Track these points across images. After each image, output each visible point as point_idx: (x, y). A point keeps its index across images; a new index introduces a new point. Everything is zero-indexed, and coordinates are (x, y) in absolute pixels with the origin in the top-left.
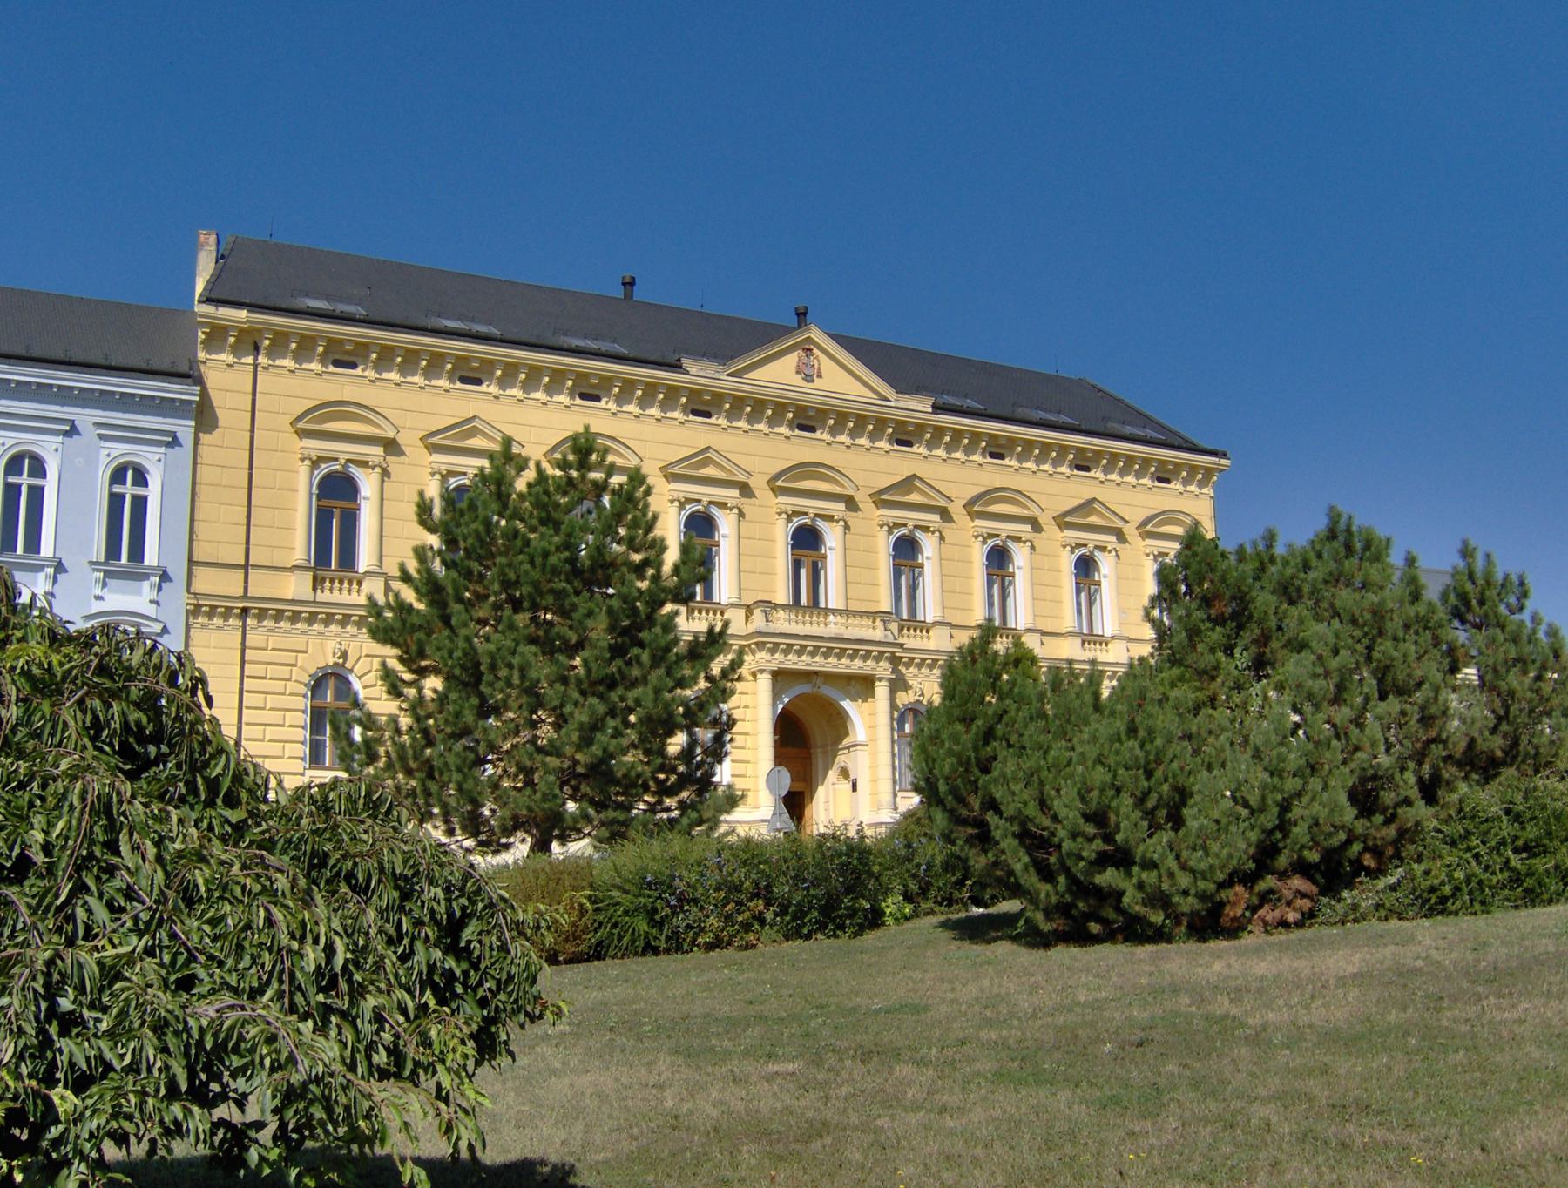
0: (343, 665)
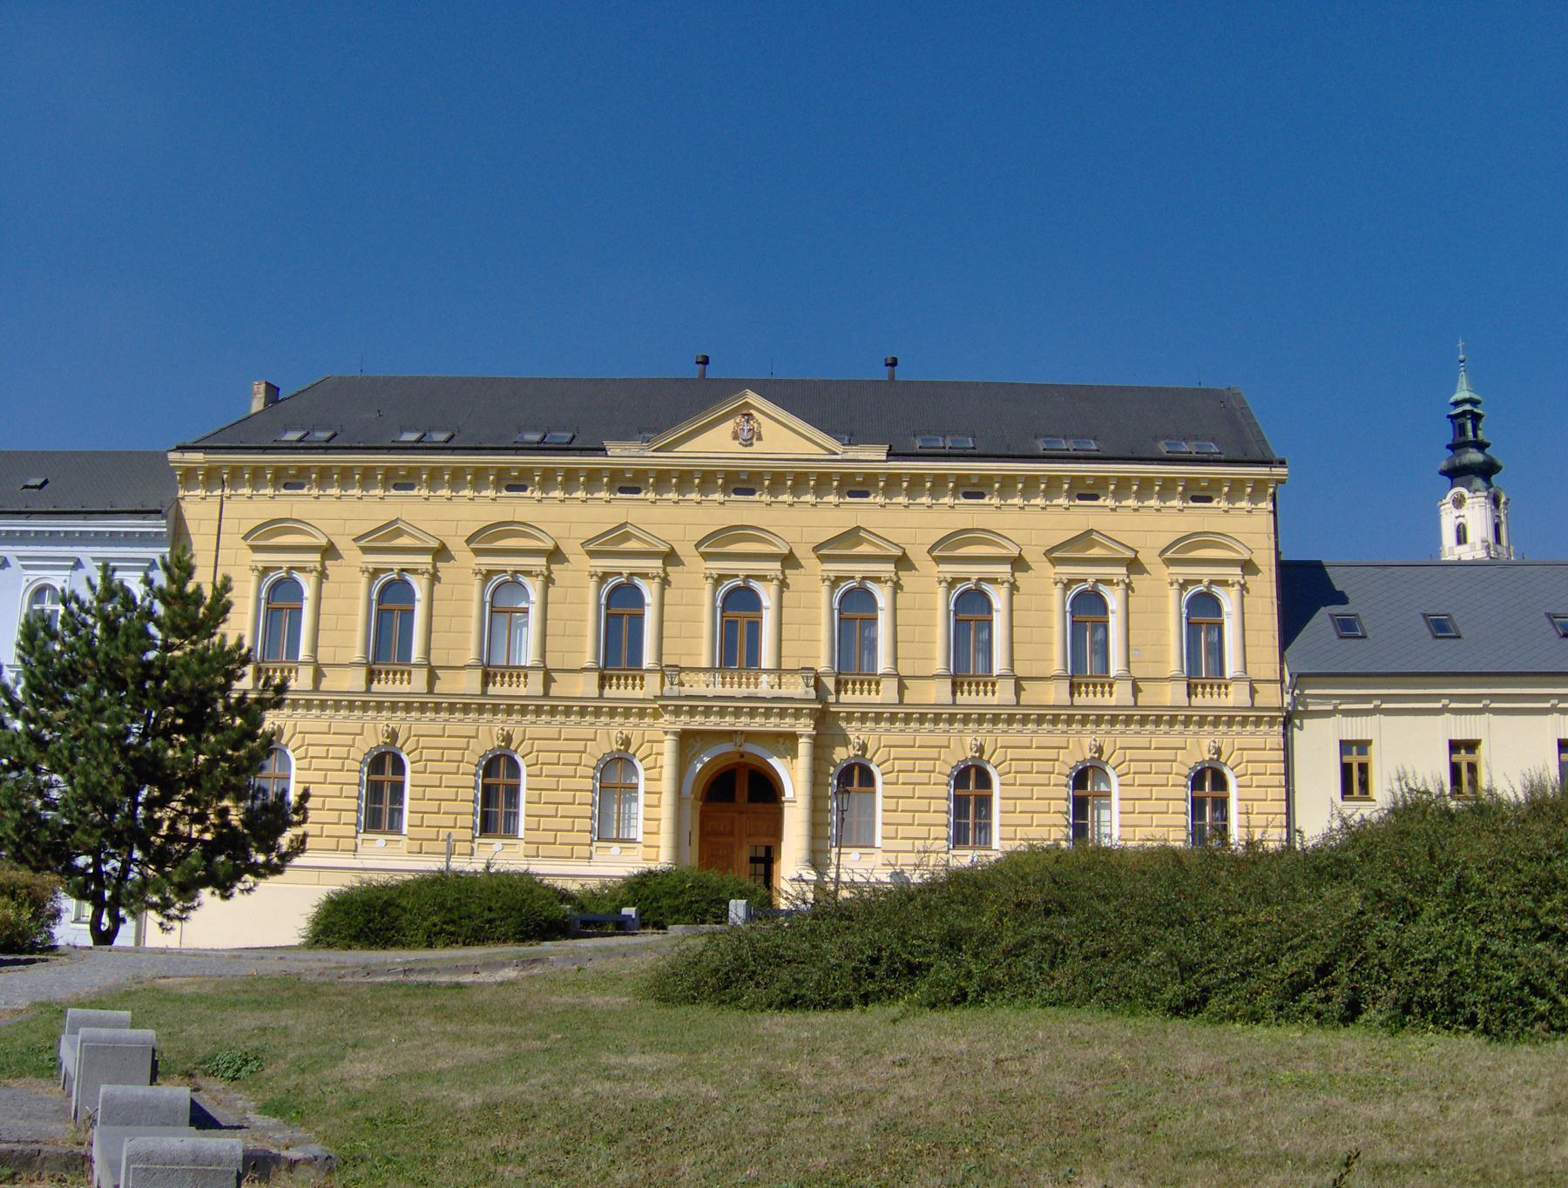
0: (981, 757)
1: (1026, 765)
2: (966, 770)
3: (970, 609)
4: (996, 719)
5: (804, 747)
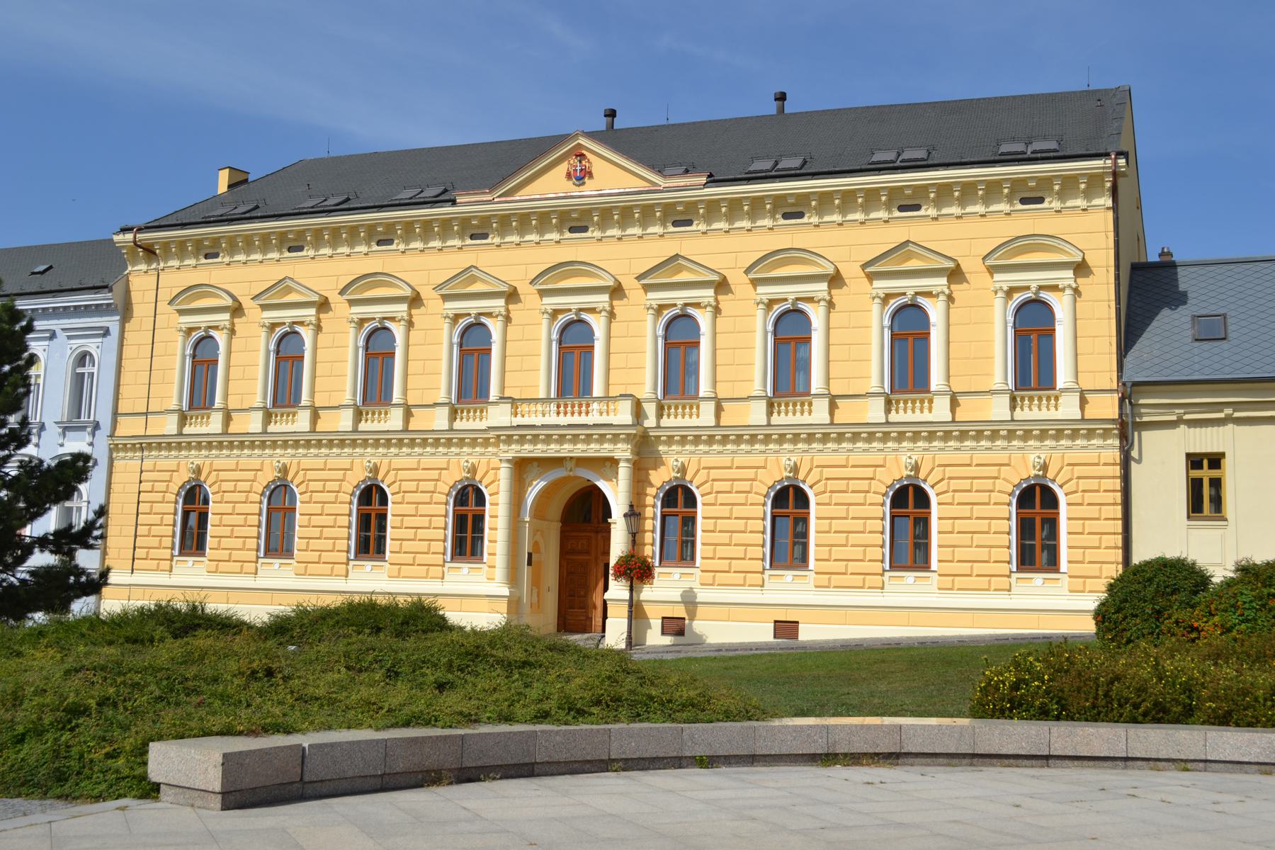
0: (1044, 476)
1: (1093, 484)
3: (790, 333)
4: (810, 438)
5: (624, 471)
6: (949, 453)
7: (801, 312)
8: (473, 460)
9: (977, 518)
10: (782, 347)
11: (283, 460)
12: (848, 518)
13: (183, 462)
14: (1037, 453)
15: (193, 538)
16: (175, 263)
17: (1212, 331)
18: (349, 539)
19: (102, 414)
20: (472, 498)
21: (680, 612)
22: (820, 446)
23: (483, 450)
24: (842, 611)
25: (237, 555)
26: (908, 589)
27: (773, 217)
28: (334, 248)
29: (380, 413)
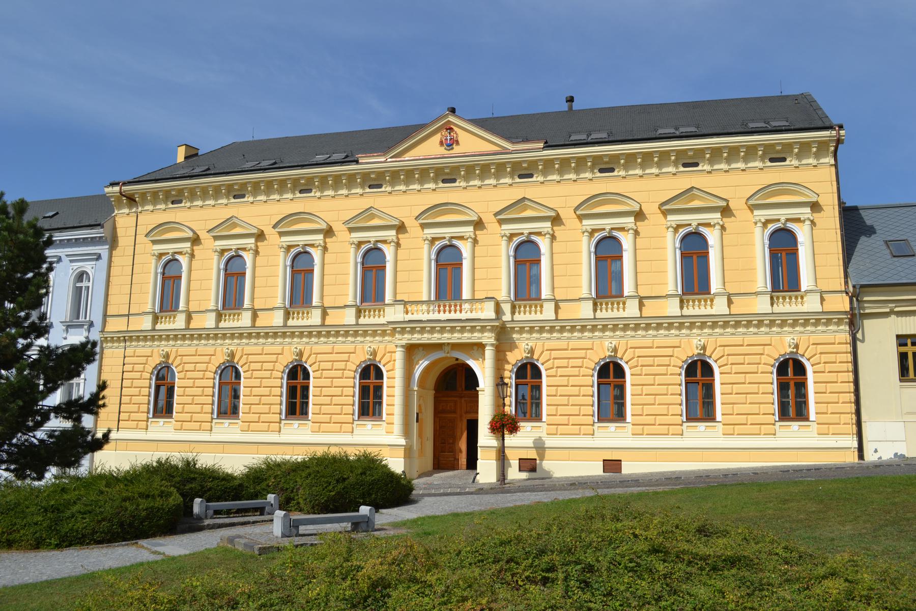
0: (704, 355)
2: (295, 367)
3: (607, 252)
4: (626, 327)
5: (489, 353)
6: (728, 336)
7: (380, 249)
8: (374, 346)
9: (749, 383)
10: (520, 267)
11: (232, 348)
12: (655, 384)
13: (156, 350)
14: (610, 340)
15: (163, 406)
16: (150, 207)
17: (900, 250)
18: (281, 404)
19: (96, 316)
20: (300, 375)
21: (532, 454)
22: (633, 333)
23: (381, 339)
24: (567, 451)
25: (196, 417)
26: (700, 435)
27: (592, 171)
28: (268, 195)
29: (303, 313)
